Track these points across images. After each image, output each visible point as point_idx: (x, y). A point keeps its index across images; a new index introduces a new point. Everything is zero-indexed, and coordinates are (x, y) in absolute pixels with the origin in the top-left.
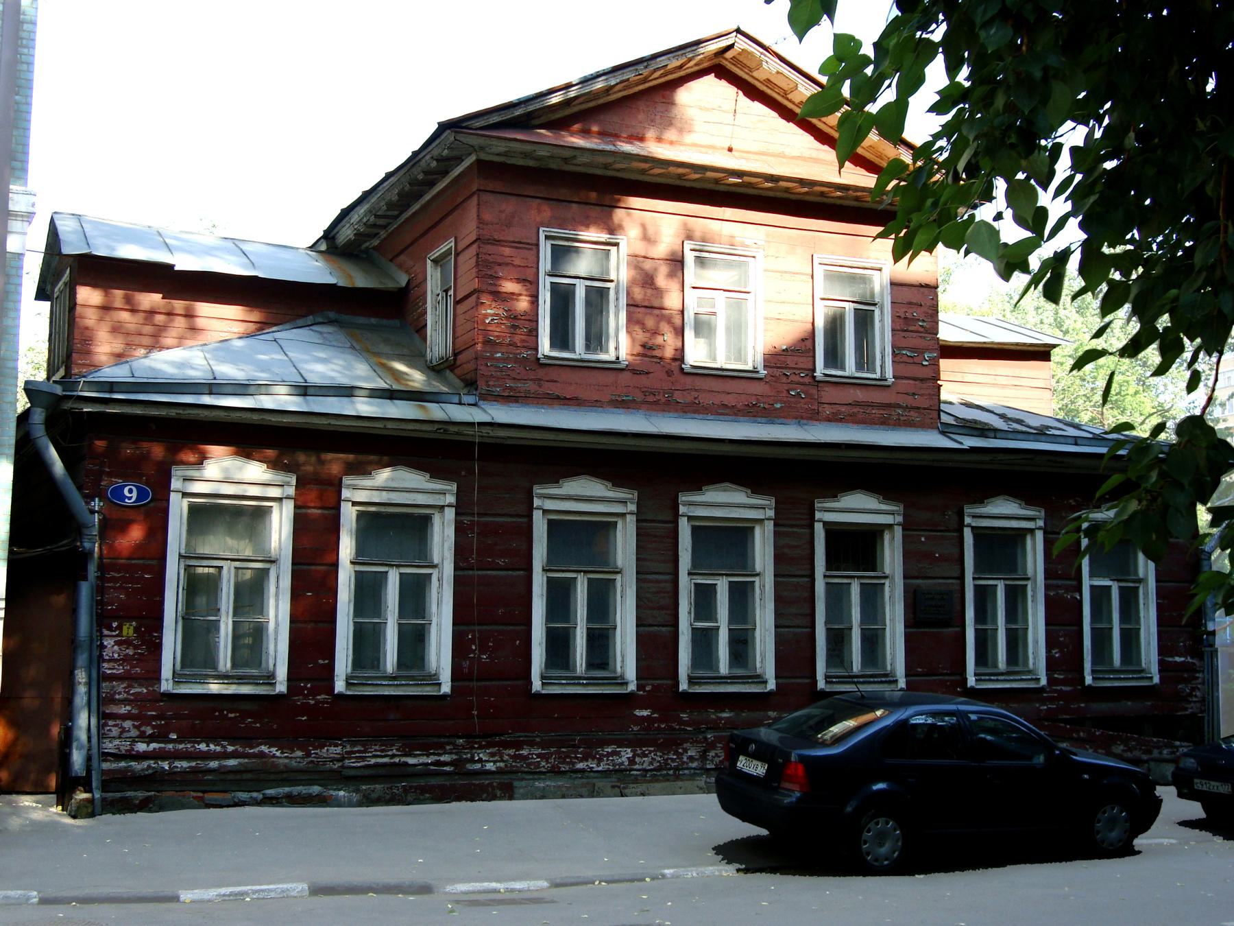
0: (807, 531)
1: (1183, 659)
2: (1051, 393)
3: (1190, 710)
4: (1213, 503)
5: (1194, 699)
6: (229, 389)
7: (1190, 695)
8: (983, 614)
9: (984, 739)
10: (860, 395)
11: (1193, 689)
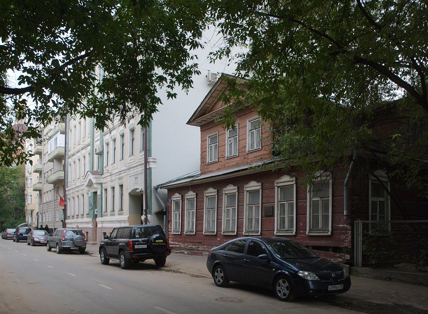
1: (343, 225)
4: (315, 277)
5: (382, 80)
6: (183, 179)
7: (345, 239)
8: (283, 211)
11: (346, 237)
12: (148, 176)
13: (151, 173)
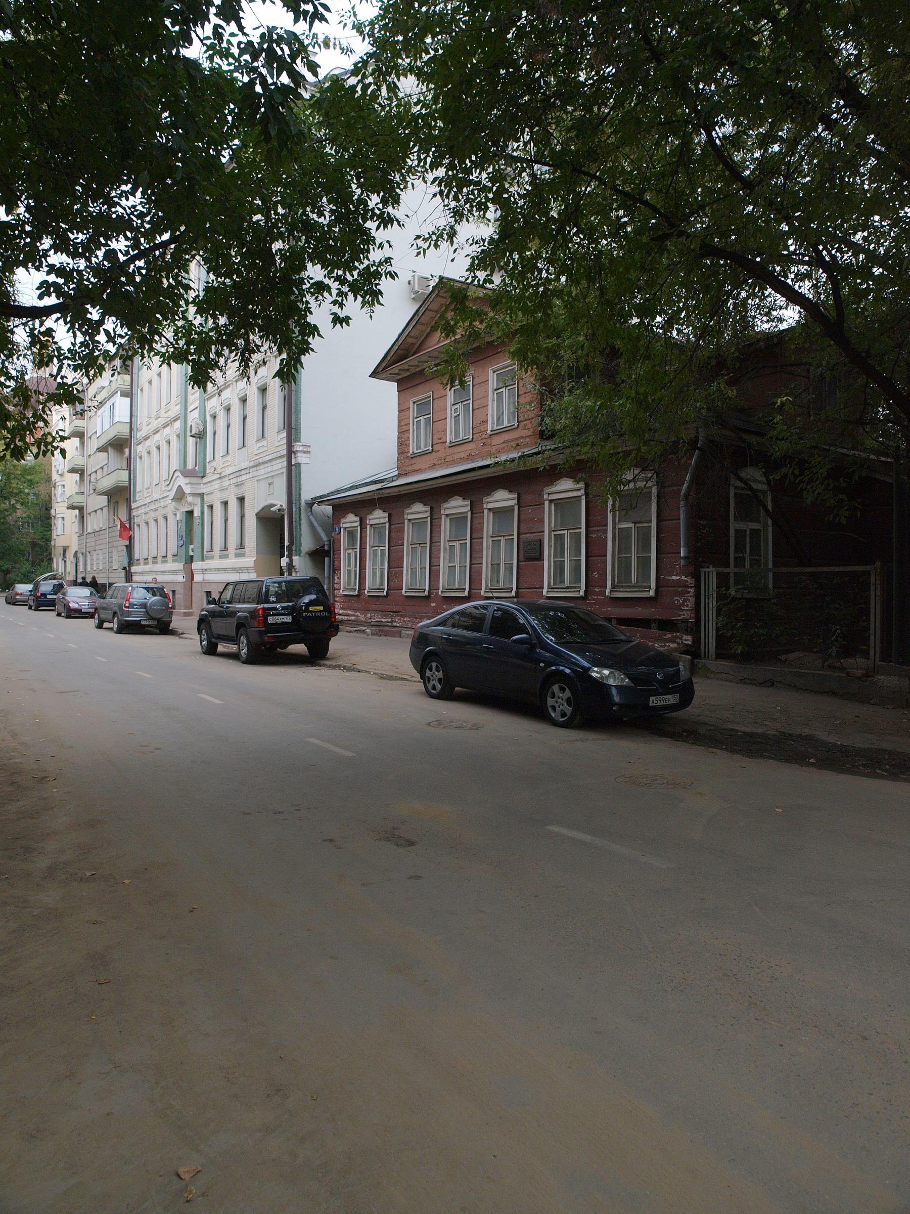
0: (473, 562)
1: (678, 578)
2: (444, 245)
3: (682, 617)
4: (623, 680)
7: (683, 605)
9: (563, 671)
10: (506, 437)
11: (685, 601)
12: (294, 480)
13: (300, 474)
